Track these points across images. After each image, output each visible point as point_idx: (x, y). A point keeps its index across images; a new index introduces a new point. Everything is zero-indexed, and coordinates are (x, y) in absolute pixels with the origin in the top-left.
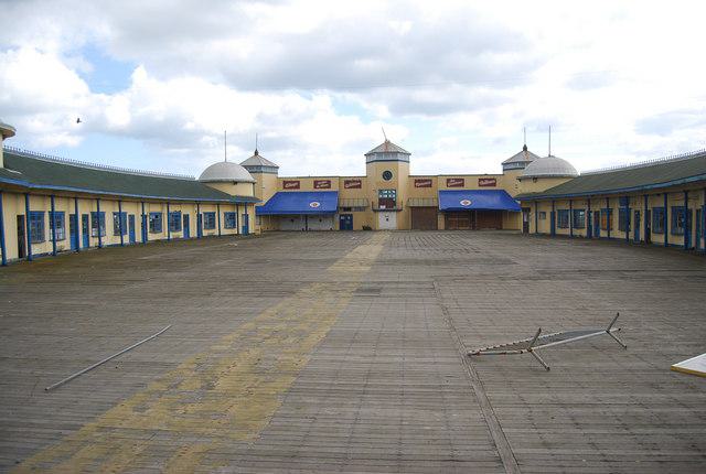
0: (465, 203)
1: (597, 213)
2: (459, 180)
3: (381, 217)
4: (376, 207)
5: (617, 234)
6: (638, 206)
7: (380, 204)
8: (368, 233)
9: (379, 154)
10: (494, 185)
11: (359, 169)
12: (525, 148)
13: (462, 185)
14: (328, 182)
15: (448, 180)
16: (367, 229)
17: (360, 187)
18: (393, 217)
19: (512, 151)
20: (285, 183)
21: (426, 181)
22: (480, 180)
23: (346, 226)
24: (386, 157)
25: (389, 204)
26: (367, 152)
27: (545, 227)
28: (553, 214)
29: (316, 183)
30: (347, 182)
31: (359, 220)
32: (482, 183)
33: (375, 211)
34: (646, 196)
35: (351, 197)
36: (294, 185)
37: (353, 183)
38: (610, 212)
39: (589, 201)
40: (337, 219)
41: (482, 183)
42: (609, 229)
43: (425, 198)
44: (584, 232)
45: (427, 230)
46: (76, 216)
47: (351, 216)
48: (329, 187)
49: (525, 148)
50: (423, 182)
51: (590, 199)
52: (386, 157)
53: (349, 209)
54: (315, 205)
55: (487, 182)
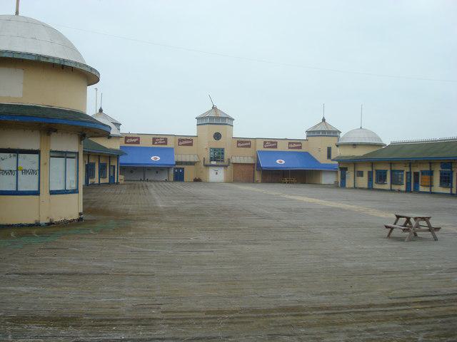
0: (280, 162)
1: (416, 174)
2: (272, 143)
3: (212, 172)
4: (208, 163)
5: (437, 188)
6: (366, 170)
7: (211, 160)
8: (198, 183)
9: (211, 118)
10: (300, 148)
11: (190, 129)
12: (324, 120)
13: (276, 147)
14: (165, 140)
15: (265, 143)
16: (197, 180)
17: (191, 144)
18: (221, 171)
19: (313, 122)
20: (126, 138)
21: (246, 142)
22: (290, 143)
23: (179, 177)
24: (215, 121)
25: (218, 157)
26: (199, 114)
27: (363, 182)
28: (370, 174)
29: (154, 140)
30: (181, 140)
31: (189, 173)
32: (291, 146)
33: (207, 166)
34: (430, 163)
35: (184, 155)
36: (135, 140)
37: (186, 141)
38: (431, 173)
39: (372, 164)
40: (172, 172)
41: (291, 146)
42: (431, 186)
43: (245, 157)
44: (403, 188)
45: (274, 182)
46: (410, 172)
47: (183, 169)
48: (166, 144)
49: (324, 120)
50: (244, 143)
51: (410, 163)
52: (215, 121)
53: (181, 163)
54: (155, 159)
55: (295, 145)
